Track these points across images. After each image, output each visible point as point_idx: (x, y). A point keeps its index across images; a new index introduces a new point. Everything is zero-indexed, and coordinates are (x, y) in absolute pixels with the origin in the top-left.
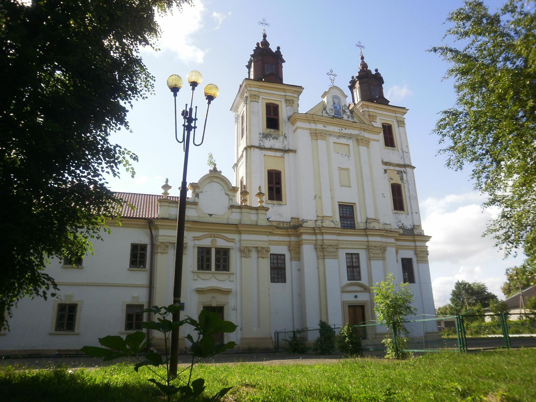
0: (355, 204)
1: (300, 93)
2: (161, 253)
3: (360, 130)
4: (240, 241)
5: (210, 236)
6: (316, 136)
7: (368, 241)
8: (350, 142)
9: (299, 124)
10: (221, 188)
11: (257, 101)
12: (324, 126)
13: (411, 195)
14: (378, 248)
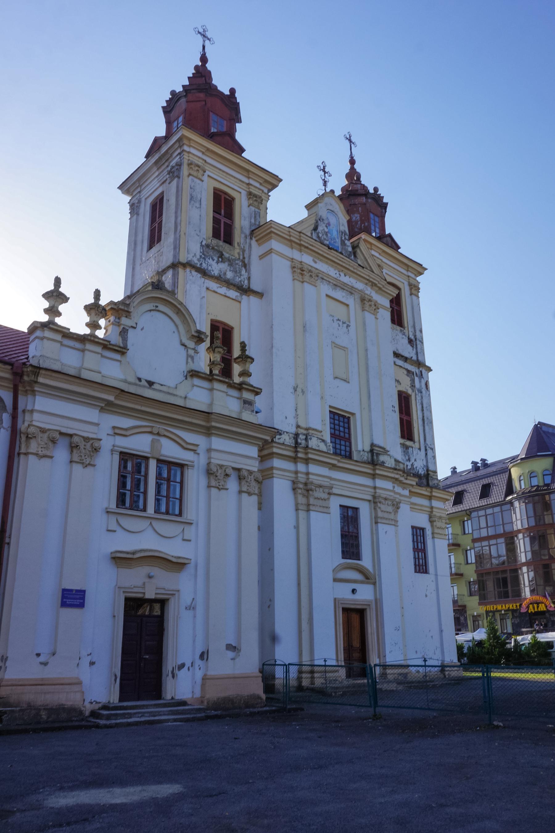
0: (353, 414)
1: (274, 186)
2: (36, 454)
3: (366, 284)
4: (209, 450)
5: (149, 430)
6: (302, 275)
7: (375, 488)
8: (350, 301)
9: (275, 244)
10: (174, 328)
11: (200, 177)
12: (313, 260)
13: (425, 415)
14: (390, 503)
